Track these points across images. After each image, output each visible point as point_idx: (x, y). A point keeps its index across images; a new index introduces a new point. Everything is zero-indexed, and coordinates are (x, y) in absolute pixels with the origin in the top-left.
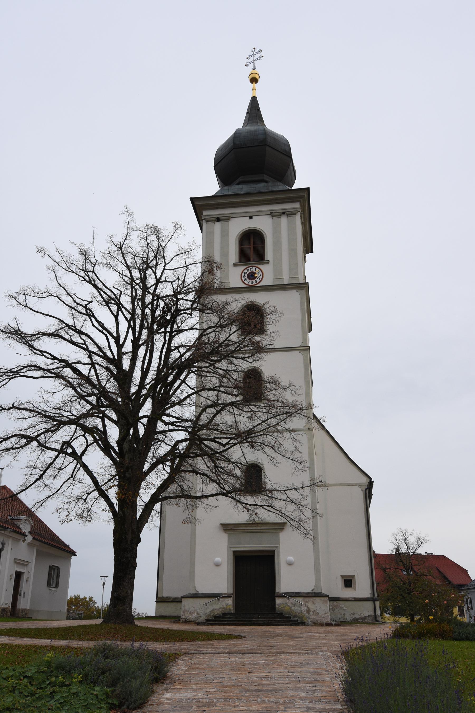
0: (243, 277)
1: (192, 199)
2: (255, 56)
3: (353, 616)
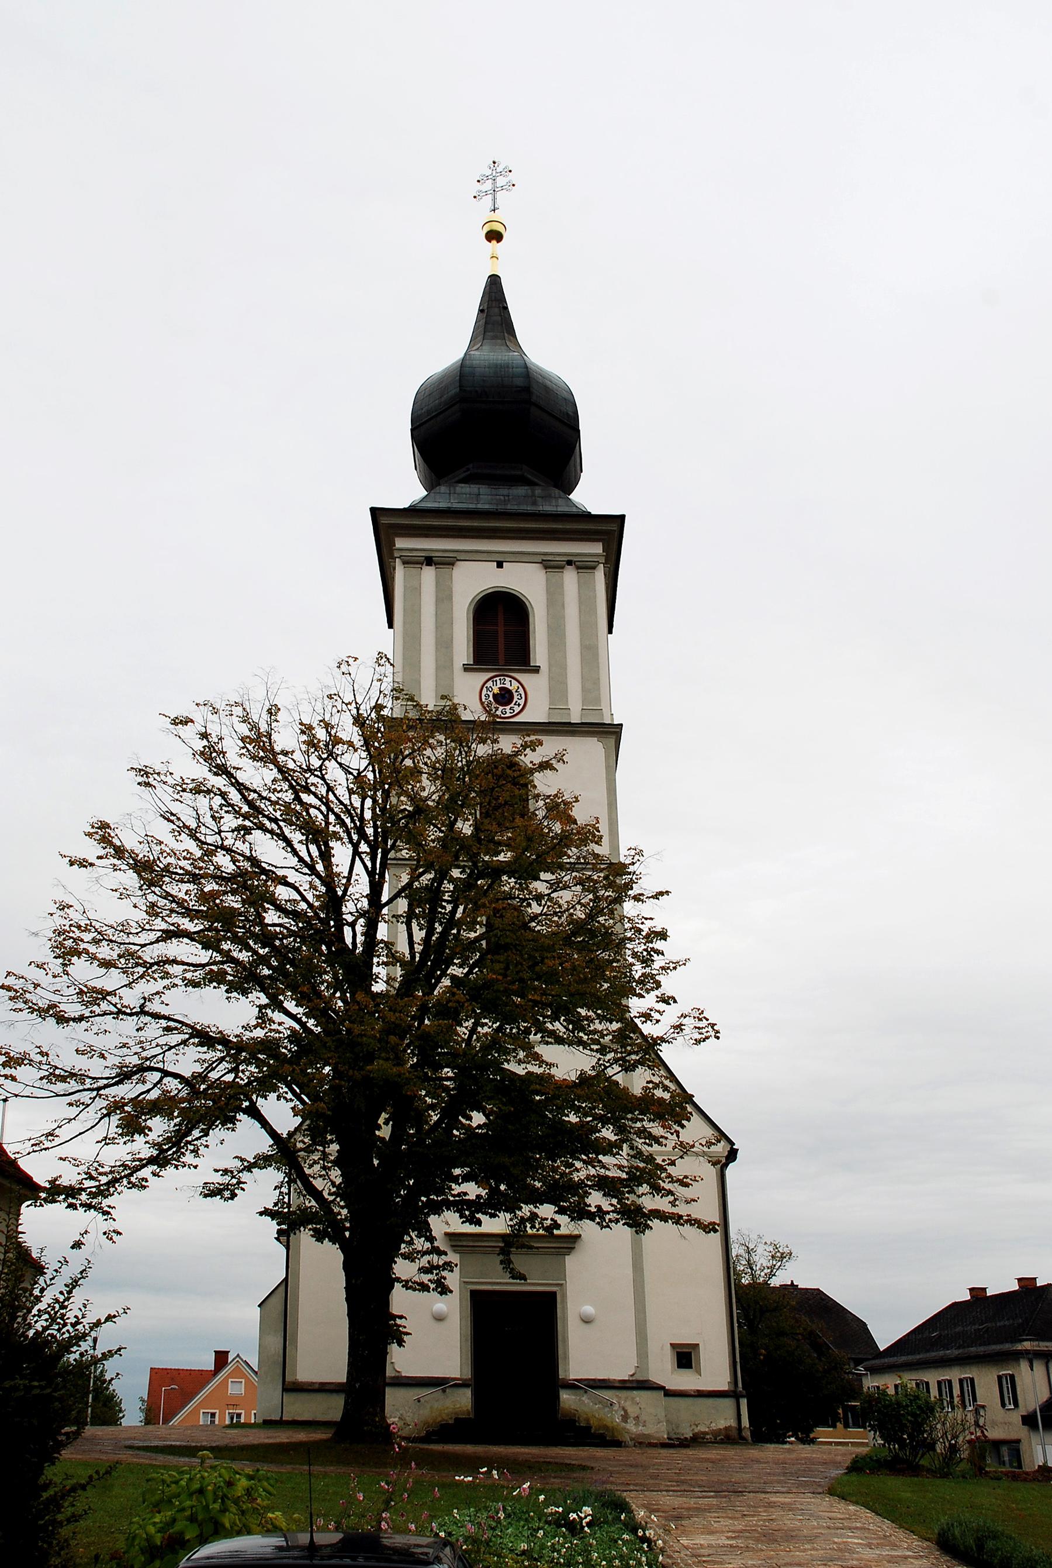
1: (375, 512)
2: (495, 180)
3: (694, 1427)
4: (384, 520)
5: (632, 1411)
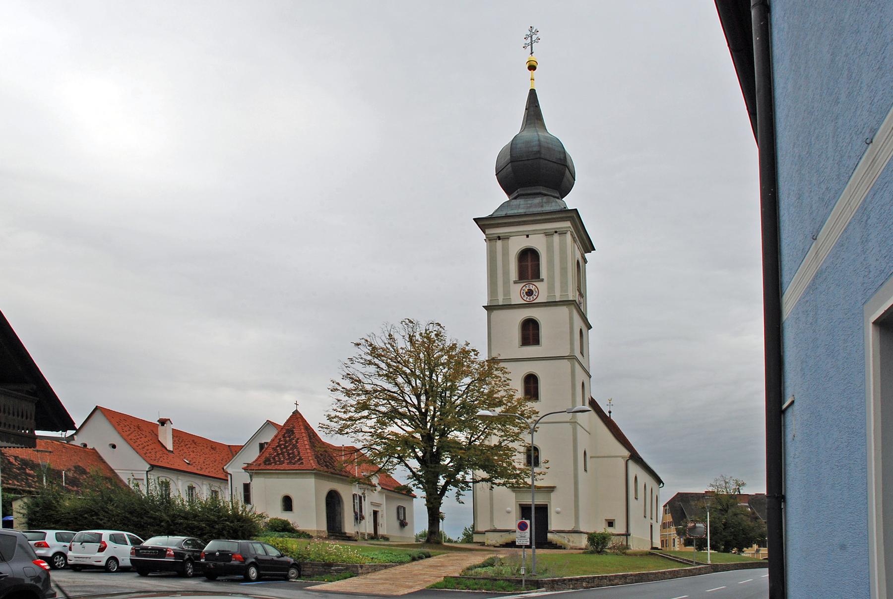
1: (475, 219)
2: (532, 38)
4: (299, 432)
5: (571, 539)
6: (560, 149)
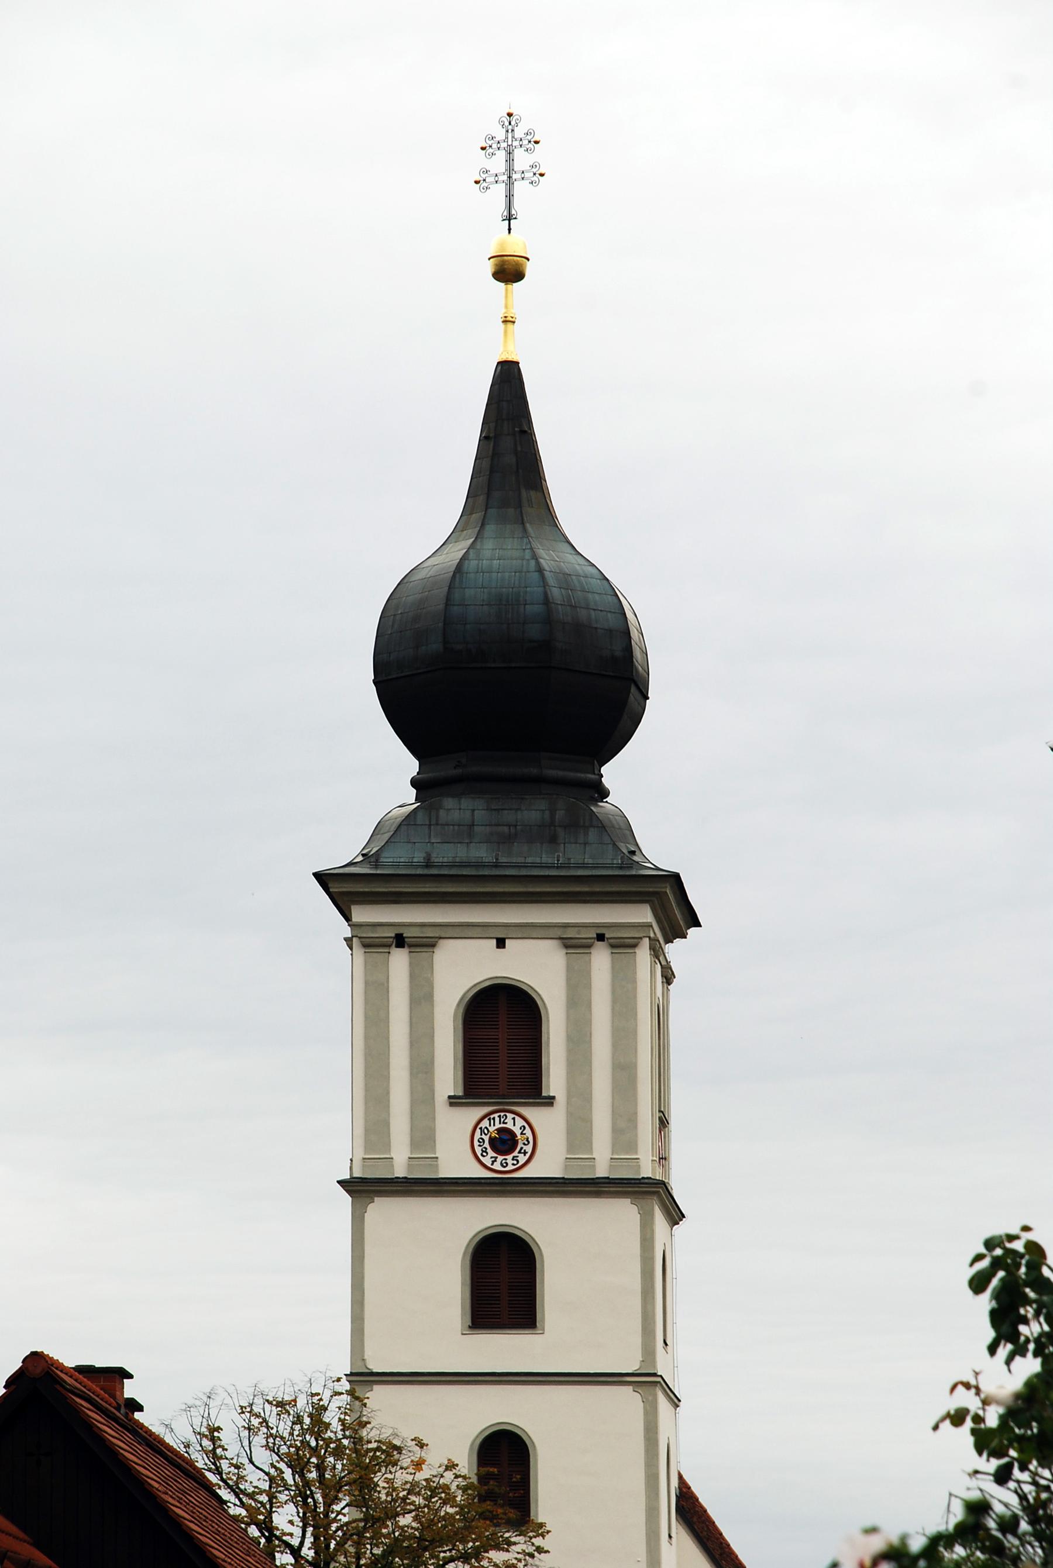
0: (476, 1143)
1: (318, 876)
4: (513, 1514)
6: (612, 621)
